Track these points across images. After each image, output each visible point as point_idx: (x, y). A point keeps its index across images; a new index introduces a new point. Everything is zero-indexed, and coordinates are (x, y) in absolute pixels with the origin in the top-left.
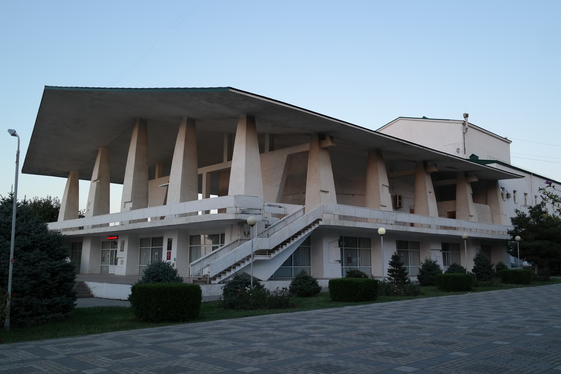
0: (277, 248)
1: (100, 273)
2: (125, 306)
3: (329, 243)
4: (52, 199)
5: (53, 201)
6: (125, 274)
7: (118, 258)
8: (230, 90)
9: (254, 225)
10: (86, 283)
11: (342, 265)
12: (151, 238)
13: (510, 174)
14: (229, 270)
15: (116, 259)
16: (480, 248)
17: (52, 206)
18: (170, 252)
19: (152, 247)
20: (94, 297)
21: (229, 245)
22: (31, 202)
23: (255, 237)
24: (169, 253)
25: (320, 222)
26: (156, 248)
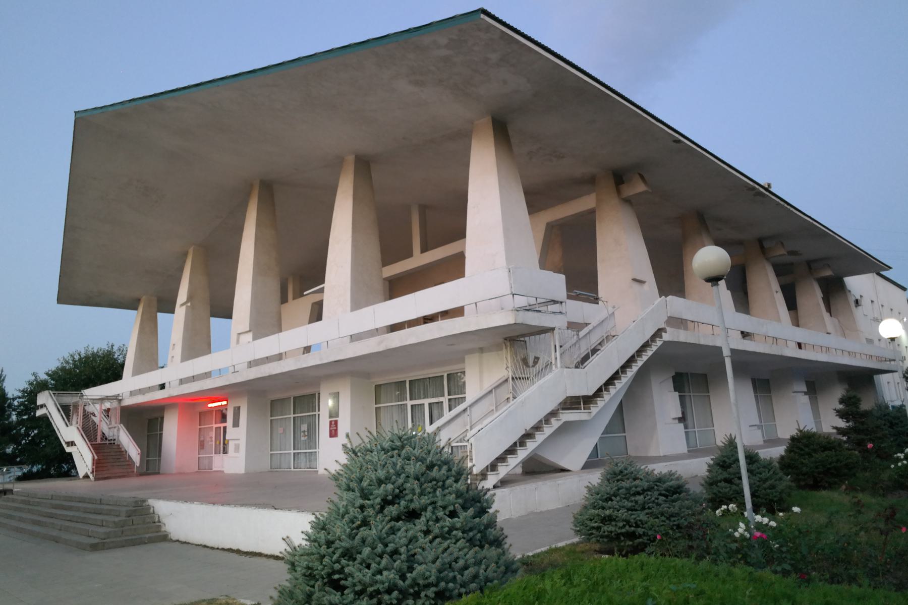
0: (598, 393)
1: (196, 469)
2: (250, 557)
3: (661, 383)
4: (115, 348)
5: (117, 352)
6: (243, 471)
7: (228, 440)
8: (482, 16)
10: (151, 502)
13: (874, 260)
14: (511, 451)
15: (226, 442)
16: (847, 386)
17: (116, 360)
18: (336, 422)
19: (294, 416)
20: (171, 541)
21: (491, 392)
22: (80, 355)
23: (556, 367)
24: (333, 423)
25: (663, 334)
26: (303, 416)
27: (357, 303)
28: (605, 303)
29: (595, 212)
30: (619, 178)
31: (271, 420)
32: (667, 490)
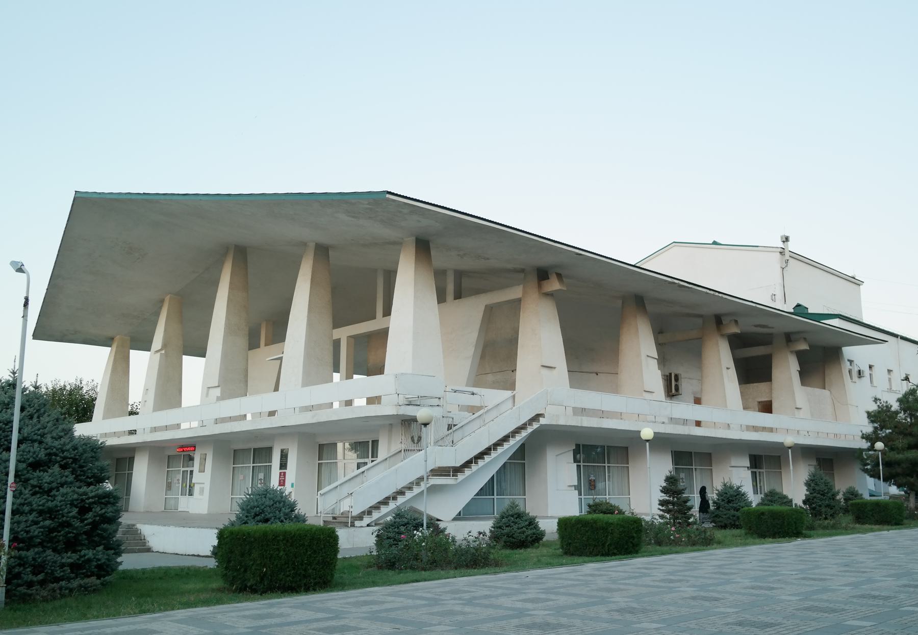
0: (468, 464)
4: (84, 383)
6: (206, 512)
7: (194, 484)
8: (388, 196)
9: (428, 424)
10: (139, 526)
11: (580, 494)
12: (251, 449)
14: (385, 502)
16: (814, 463)
18: (285, 473)
24: (282, 474)
27: (311, 377)
28: (482, 396)
29: (521, 300)
30: (543, 275)
31: (233, 467)
32: (416, 524)
